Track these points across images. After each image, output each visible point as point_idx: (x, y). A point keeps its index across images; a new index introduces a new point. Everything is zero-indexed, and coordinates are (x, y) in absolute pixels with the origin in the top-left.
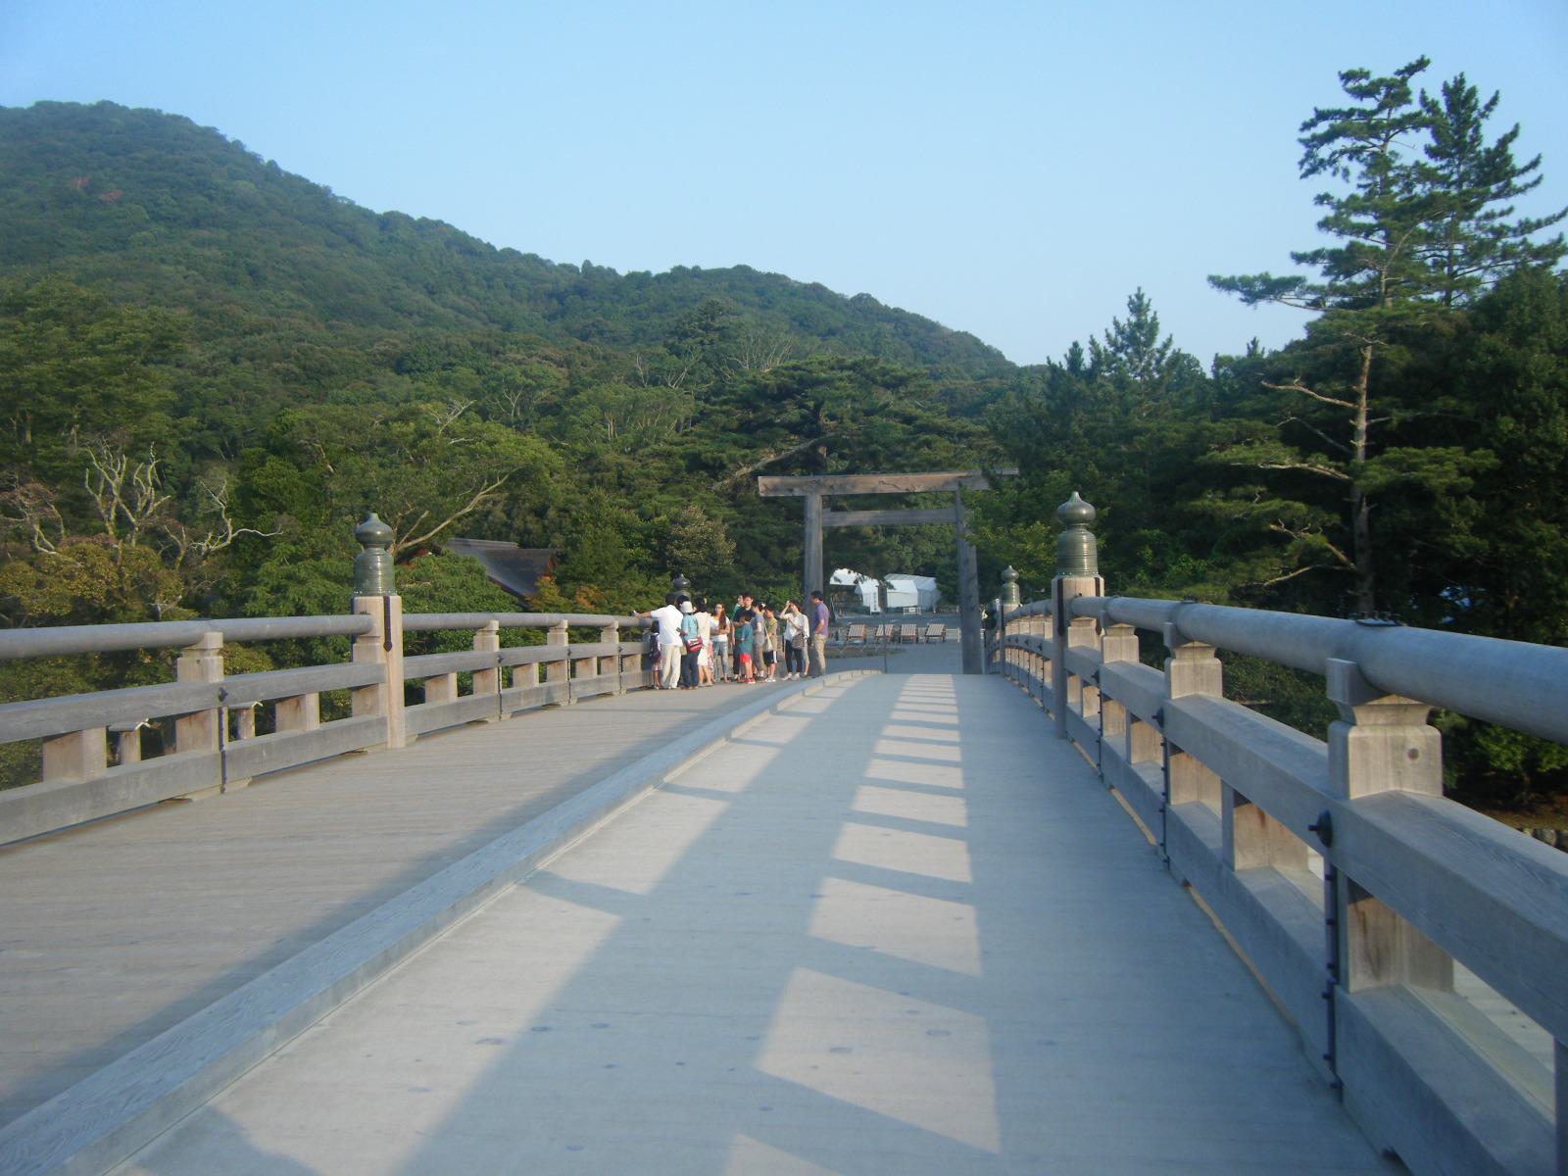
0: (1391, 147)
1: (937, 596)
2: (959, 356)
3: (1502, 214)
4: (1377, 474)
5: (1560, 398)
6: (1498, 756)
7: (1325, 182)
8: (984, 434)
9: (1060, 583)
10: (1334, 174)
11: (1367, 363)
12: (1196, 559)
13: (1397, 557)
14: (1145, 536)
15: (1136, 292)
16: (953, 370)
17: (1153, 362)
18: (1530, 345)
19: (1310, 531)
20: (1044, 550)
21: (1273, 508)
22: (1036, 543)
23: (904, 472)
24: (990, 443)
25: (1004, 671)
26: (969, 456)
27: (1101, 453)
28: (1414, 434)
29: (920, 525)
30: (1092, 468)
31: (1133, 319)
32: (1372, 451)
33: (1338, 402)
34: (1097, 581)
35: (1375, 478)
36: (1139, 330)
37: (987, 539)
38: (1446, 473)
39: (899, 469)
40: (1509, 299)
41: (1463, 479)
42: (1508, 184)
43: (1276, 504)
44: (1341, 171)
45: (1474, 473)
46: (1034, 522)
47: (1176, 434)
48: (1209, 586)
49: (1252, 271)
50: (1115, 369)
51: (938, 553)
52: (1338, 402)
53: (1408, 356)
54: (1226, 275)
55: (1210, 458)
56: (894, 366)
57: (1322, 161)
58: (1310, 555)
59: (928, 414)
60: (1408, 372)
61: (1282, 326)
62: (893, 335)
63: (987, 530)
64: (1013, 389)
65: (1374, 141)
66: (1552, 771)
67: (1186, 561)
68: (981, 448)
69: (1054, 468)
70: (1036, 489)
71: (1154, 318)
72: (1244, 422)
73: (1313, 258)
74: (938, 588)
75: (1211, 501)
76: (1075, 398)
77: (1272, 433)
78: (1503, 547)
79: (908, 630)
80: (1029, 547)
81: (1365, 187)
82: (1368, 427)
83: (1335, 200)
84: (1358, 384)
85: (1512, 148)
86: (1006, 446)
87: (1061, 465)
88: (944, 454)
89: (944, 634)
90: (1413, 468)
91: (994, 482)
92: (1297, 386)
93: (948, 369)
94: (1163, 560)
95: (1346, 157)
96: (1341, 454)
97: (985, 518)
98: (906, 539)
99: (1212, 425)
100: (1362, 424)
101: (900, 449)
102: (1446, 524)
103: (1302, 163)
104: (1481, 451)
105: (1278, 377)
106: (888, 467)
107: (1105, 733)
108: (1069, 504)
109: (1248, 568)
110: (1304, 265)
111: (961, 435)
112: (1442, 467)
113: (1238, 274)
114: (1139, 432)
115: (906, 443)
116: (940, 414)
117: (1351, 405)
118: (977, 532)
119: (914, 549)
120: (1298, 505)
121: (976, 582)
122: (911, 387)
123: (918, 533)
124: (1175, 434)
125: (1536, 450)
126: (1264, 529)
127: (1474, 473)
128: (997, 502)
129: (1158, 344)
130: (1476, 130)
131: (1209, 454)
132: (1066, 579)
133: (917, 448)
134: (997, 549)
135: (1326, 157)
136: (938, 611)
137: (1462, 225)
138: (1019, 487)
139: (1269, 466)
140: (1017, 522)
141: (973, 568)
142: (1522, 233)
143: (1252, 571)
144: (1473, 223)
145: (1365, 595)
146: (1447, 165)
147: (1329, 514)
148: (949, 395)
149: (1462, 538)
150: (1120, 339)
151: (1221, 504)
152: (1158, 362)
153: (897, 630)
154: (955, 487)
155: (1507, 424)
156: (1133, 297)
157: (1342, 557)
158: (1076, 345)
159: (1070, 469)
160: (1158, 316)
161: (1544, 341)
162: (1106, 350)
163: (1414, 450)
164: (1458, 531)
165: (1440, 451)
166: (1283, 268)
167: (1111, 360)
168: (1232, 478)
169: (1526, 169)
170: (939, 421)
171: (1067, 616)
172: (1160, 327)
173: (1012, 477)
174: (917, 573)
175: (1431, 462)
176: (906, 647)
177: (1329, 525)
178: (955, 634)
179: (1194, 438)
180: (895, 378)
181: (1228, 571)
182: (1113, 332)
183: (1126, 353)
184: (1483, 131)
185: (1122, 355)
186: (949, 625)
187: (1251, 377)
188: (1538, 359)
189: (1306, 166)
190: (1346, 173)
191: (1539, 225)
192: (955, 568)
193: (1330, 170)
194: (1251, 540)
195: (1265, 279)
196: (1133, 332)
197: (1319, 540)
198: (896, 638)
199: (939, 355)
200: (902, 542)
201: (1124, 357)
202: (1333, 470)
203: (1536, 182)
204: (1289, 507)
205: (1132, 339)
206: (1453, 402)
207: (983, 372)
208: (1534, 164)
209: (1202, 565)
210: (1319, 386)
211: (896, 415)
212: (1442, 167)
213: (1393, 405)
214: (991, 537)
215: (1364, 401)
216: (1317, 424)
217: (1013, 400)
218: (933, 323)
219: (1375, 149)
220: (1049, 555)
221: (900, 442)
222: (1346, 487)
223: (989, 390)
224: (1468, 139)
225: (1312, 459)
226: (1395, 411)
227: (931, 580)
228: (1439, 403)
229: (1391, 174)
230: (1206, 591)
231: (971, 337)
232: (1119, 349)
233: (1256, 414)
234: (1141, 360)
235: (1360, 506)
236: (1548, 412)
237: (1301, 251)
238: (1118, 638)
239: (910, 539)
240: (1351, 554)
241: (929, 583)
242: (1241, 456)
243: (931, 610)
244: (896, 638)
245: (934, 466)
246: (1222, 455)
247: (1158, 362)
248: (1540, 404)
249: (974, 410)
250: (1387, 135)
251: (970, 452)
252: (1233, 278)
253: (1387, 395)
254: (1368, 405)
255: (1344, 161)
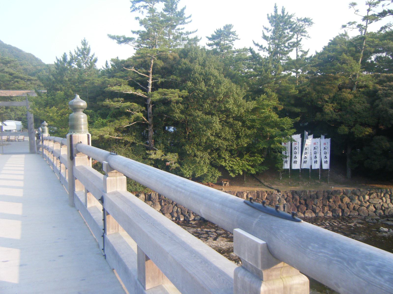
0: (154, 7)
1: (22, 127)
2: (28, 60)
3: (182, 29)
4: (156, 96)
5: (202, 78)
6: (186, 174)
7: (137, 14)
8: (36, 80)
9: (71, 136)
10: (139, 12)
11: (152, 64)
12: (103, 119)
13: (160, 120)
14: (88, 112)
15: (84, 39)
16: (26, 63)
17: (89, 60)
18: (195, 63)
19: (137, 112)
20: (56, 115)
21: (128, 105)
22: (53, 113)
23: (10, 90)
24: (38, 82)
25: (44, 156)
26: (31, 86)
27: (74, 86)
28: (164, 85)
29: (17, 106)
30: (71, 91)
31: (83, 47)
32: (153, 90)
33: (144, 75)
34: (88, 135)
35: (156, 97)
36: (85, 51)
37: (37, 112)
38: (176, 96)
39: (8, 89)
40: (189, 50)
41: (180, 98)
42: (184, 21)
43: (128, 104)
44: (141, 12)
45: (182, 97)
46: (52, 107)
47: (98, 81)
48: (108, 128)
49: (120, 34)
50: (77, 61)
51: (22, 114)
52: (144, 75)
53: (163, 63)
54: (113, 34)
55: (109, 89)
56: (6, 57)
57: (136, 8)
58: (137, 118)
59: (18, 73)
60: (163, 68)
61: (127, 52)
62: (8, 52)
63: (37, 109)
64: (44, 69)
65: (151, 4)
66: (199, 177)
67: (100, 120)
68: (35, 84)
69: (58, 90)
70: (53, 96)
71: (89, 47)
72: (118, 79)
73: (138, 32)
74: (23, 125)
75: (107, 102)
76: (65, 69)
77: (125, 83)
78: (188, 117)
79: (12, 138)
80: (51, 114)
81: (148, 17)
82: (152, 83)
83: (140, 19)
84: (149, 70)
85: (185, 11)
86: (43, 83)
87: (61, 90)
88: (23, 85)
89: (24, 139)
90: (165, 94)
91: (39, 94)
92: (133, 69)
93: (25, 63)
94: (93, 119)
95: (143, 8)
96: (145, 90)
97: (36, 105)
98: (12, 110)
99: (109, 80)
100: (150, 82)
101: (8, 82)
102: (174, 111)
103: (131, 8)
104: (184, 91)
105: (128, 66)
106: (4, 88)
107: (108, 233)
108: (75, 100)
109: (119, 122)
110: (135, 34)
111: (28, 80)
112: (174, 95)
113: (116, 35)
114: (86, 80)
115: (10, 81)
116: (21, 73)
117: (147, 76)
118: (33, 109)
119: (15, 113)
120: (135, 104)
121: (33, 124)
122: (12, 64)
123: (16, 108)
124: (97, 81)
125: (197, 91)
126: (125, 111)
127: (182, 97)
128: (40, 100)
129: (90, 55)
130: (176, 5)
131: (109, 88)
132: (74, 135)
133: (14, 83)
134: (40, 115)
135: (137, 7)
136: (22, 131)
137: (172, 31)
138: (47, 96)
139: (126, 92)
140: (47, 107)
141: (33, 120)
142: (187, 35)
143: (120, 123)
144: (174, 30)
145: (151, 130)
146: (169, 14)
147: (142, 107)
148: (25, 70)
149: (177, 115)
150: (79, 53)
151: (112, 103)
152: (91, 60)
153: (8, 137)
154: (26, 95)
155: (189, 84)
156: (83, 41)
157: (145, 120)
158: (65, 53)
159: (64, 91)
160: (90, 46)
161: (198, 62)
162: (74, 56)
163: (166, 90)
164: (176, 113)
165: (173, 90)
166: (129, 35)
167: (76, 59)
168: (113, 95)
169: (188, 18)
170: (21, 75)
171: (74, 152)
172: (91, 50)
173: (45, 93)
174: (16, 120)
175: (171, 93)
176: (11, 143)
177: (142, 110)
178: (27, 139)
179: (103, 83)
180: (6, 61)
181: (113, 123)
182: (77, 50)
183: (81, 57)
184: (178, 6)
185: (79, 57)
186: (25, 135)
187: (120, 67)
188: (197, 67)
189: (132, 9)
190: (143, 12)
191: (191, 33)
192: (27, 119)
193: (138, 11)
194: (120, 114)
195: (124, 37)
196: (83, 51)
197: (141, 115)
198: (8, 140)
199: (22, 59)
200: (11, 111)
201: (80, 58)
202: (143, 94)
203: (190, 22)
204: (133, 105)
205: (83, 53)
206: (175, 77)
207: (36, 65)
208: (190, 17)
209: (105, 121)
210: (139, 70)
211: (7, 73)
212: (167, 14)
213: (158, 77)
214: (38, 111)
215: (151, 75)
216: (138, 81)
217: (44, 73)
218: (20, 50)
219: (151, 7)
220: (57, 117)
221: (8, 81)
222: (146, 100)
223: (37, 69)
224: (174, 7)
225: (137, 91)
226: (159, 79)
227: (20, 122)
228: (171, 77)
229: (155, 14)
230: (107, 129)
231: (32, 55)
232: (79, 55)
233: (121, 77)
234: (85, 59)
235: (150, 105)
236: (200, 82)
237: (134, 30)
238: (115, 178)
239: (13, 110)
240: (147, 118)
241: (20, 123)
242: (118, 89)
243: (20, 131)
244: (8, 140)
245: (20, 89)
246: (113, 88)
247: (91, 60)
248: (198, 79)
249: (33, 75)
250: (154, 2)
251: (31, 85)
252: (115, 36)
253: (157, 74)
254: (152, 76)
255: (142, 9)
